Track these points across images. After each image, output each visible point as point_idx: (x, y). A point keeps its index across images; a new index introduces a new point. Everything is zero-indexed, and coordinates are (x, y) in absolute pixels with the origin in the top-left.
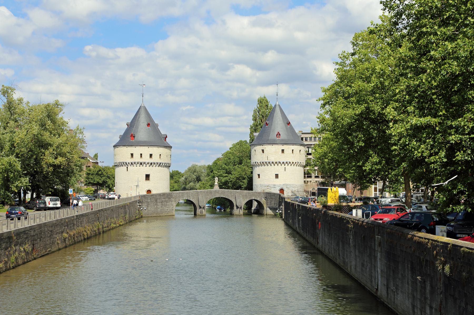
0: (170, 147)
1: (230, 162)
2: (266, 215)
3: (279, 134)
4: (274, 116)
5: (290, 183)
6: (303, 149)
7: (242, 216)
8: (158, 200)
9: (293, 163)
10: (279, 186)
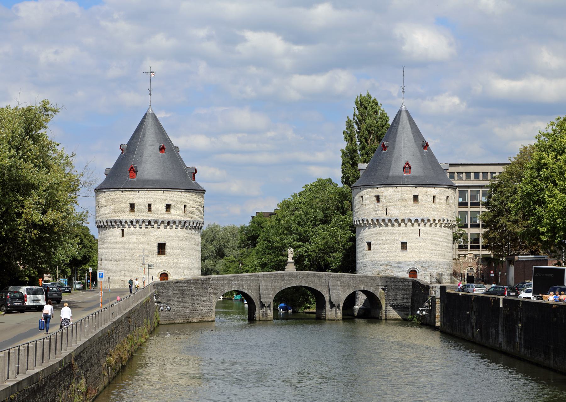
0: (200, 191)
1: (308, 219)
2: (386, 319)
3: (407, 167)
4: (399, 132)
5: (428, 260)
6: (454, 195)
7: (341, 321)
8: (187, 293)
9: (434, 220)
10: (408, 265)
